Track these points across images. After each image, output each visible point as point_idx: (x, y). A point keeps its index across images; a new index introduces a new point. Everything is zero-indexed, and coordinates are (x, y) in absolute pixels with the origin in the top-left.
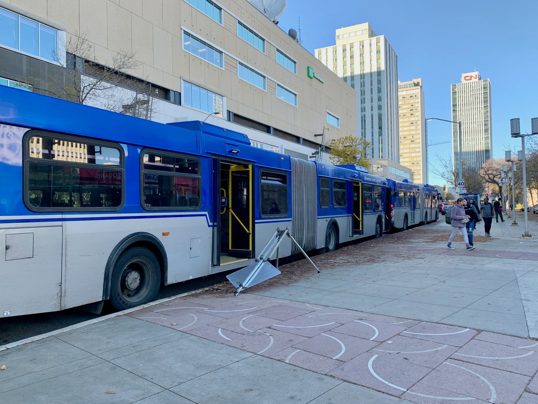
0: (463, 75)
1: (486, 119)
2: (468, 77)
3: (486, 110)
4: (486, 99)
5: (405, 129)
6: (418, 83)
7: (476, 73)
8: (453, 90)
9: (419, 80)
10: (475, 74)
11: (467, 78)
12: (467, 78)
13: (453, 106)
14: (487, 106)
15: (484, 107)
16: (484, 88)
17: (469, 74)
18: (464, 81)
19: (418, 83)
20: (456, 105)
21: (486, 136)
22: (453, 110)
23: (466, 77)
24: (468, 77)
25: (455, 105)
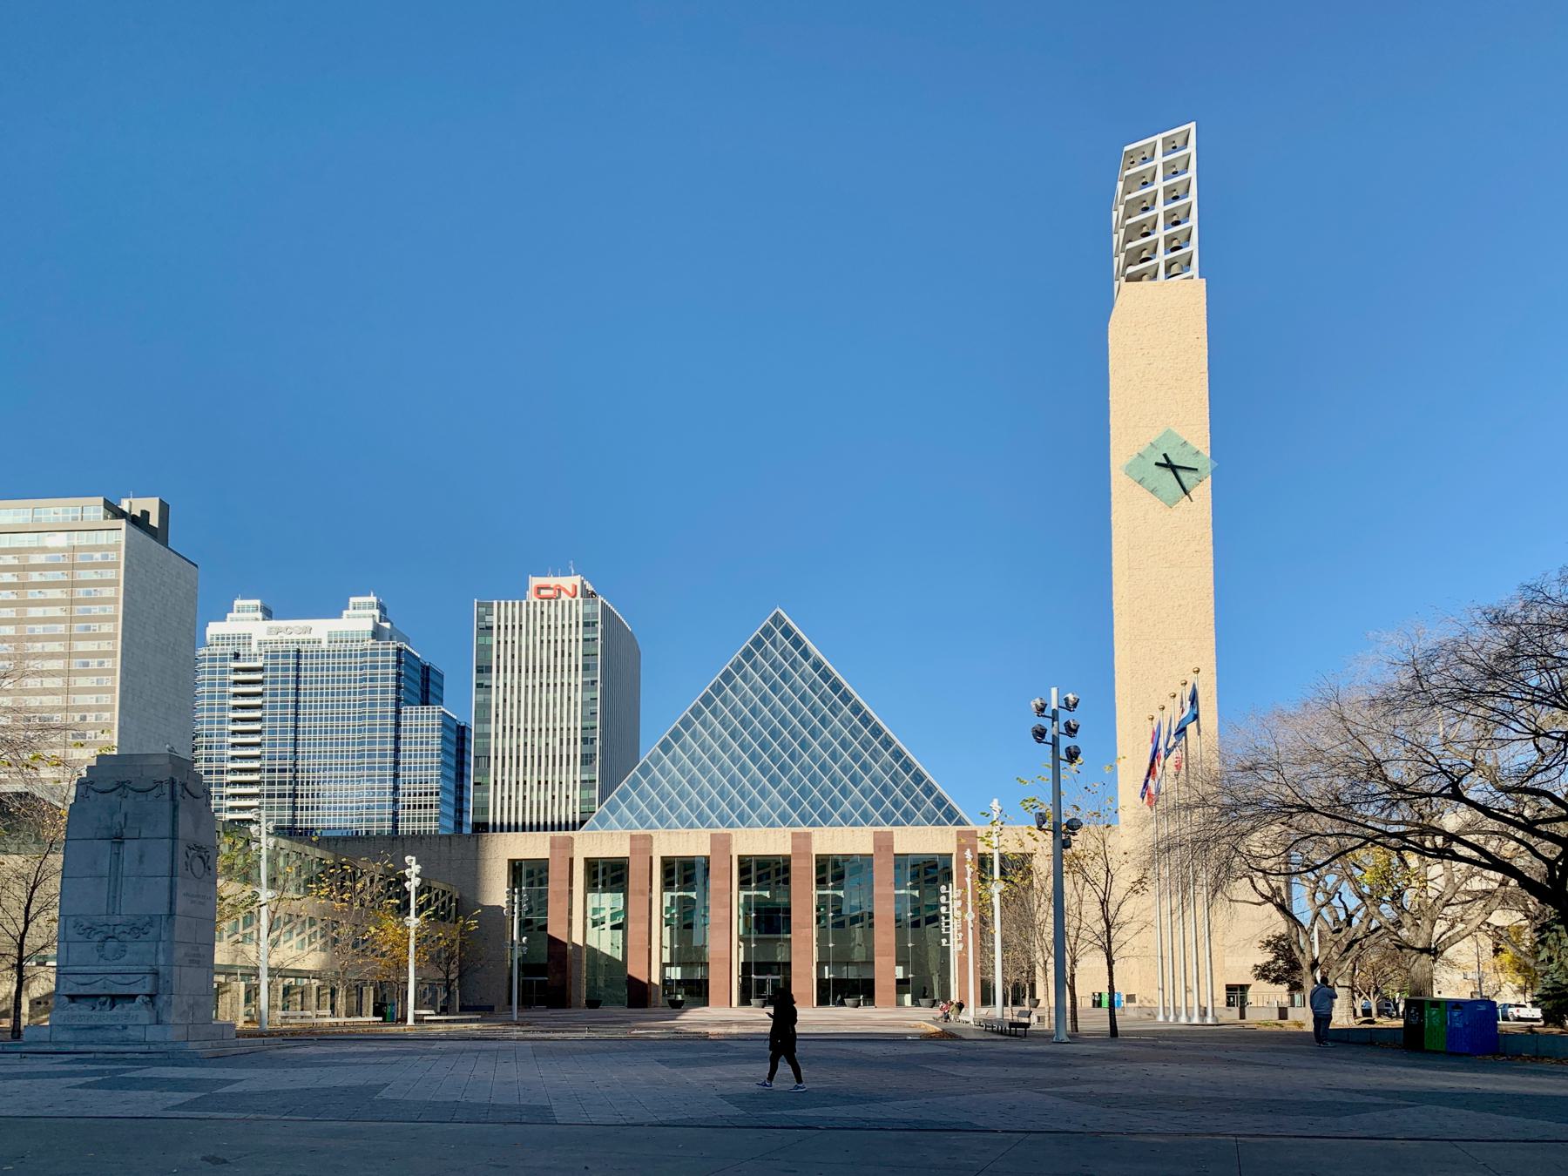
0: (535, 581)
1: (587, 724)
2: (548, 588)
3: (589, 695)
4: (590, 661)
5: (50, 683)
6: (146, 514)
7: (577, 580)
8: (481, 618)
9: (152, 505)
10: (571, 582)
11: (543, 592)
12: (543, 592)
13: (480, 670)
14: (594, 682)
15: (584, 683)
16: (586, 625)
17: (552, 581)
18: (532, 598)
19: (146, 514)
20: (489, 669)
21: (586, 777)
22: (478, 686)
23: (539, 589)
24: (548, 588)
25: (484, 669)
